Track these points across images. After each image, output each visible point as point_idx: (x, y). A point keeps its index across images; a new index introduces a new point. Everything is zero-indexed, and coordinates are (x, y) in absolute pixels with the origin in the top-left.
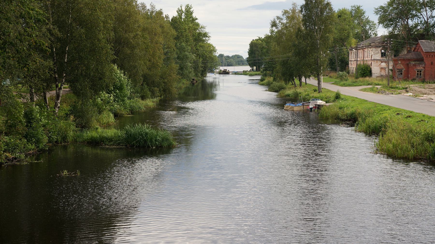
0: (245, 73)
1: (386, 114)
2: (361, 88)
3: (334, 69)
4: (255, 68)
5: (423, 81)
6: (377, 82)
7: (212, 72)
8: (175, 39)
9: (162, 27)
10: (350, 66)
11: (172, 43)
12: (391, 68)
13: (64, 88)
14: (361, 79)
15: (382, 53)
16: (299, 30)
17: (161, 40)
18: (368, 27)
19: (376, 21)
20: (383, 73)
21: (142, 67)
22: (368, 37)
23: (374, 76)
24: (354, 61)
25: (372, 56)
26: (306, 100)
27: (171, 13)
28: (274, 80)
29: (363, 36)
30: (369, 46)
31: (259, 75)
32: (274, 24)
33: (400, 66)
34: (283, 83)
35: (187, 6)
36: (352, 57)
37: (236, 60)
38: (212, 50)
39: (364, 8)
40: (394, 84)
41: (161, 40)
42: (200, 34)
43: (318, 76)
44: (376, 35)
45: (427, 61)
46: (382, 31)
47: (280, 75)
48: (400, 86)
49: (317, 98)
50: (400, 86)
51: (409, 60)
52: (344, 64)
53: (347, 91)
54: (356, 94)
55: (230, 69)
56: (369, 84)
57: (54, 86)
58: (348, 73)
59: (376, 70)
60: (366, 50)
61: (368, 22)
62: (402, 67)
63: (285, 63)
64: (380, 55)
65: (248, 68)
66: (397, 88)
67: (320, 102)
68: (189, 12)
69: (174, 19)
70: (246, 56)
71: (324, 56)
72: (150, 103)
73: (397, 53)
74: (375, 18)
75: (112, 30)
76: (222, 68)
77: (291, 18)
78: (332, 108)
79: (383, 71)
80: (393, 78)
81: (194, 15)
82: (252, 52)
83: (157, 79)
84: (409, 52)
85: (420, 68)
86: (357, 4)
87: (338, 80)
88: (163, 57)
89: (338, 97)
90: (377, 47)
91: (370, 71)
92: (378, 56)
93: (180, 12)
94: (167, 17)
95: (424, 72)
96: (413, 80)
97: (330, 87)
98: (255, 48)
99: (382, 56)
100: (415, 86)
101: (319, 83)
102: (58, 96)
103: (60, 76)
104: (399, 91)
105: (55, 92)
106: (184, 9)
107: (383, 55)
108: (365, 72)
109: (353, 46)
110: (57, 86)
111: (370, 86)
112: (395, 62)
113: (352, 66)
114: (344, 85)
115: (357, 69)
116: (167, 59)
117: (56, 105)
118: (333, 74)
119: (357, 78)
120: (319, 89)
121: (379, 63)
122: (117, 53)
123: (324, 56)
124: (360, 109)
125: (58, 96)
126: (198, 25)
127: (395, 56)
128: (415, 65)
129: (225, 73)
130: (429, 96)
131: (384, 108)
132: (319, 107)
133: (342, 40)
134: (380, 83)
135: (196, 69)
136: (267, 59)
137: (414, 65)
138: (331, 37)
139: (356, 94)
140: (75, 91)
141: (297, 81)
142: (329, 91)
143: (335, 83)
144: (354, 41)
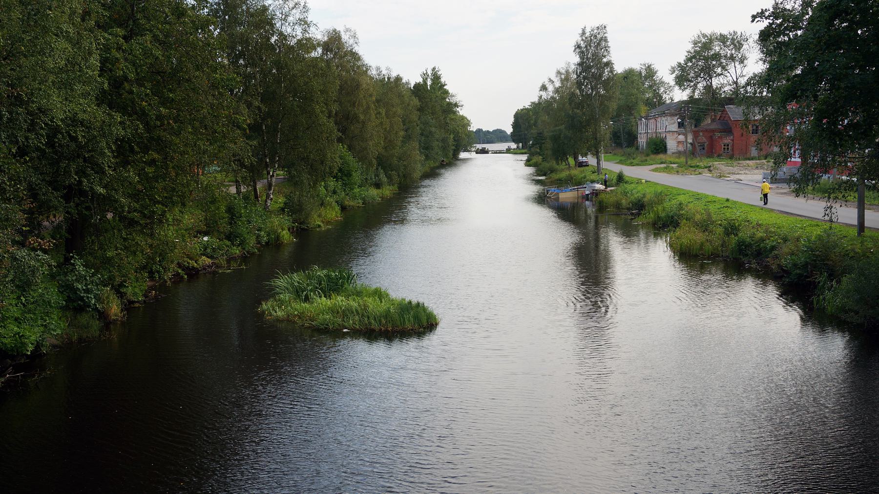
0: (508, 151)
1: (681, 198)
2: (654, 167)
3: (619, 145)
4: (521, 145)
5: (731, 158)
6: (672, 160)
7: (466, 150)
8: (419, 110)
9: (400, 96)
10: (639, 140)
11: (414, 116)
12: (690, 140)
13: (278, 175)
14: (653, 156)
15: (679, 123)
16: (573, 94)
17: (400, 111)
18: (662, 89)
19: (672, 83)
20: (681, 148)
21: (374, 146)
22: (661, 102)
23: (669, 152)
24: (644, 132)
25: (668, 126)
26: (579, 183)
27: (412, 78)
28: (544, 160)
29: (656, 104)
30: (663, 114)
31: (525, 153)
32: (544, 88)
33: (702, 139)
34: (553, 163)
35: (434, 69)
36: (641, 129)
37: (498, 136)
38: (464, 122)
39: (655, 67)
40: (695, 162)
41: (400, 111)
42: (450, 104)
43: (597, 154)
44: (672, 100)
45: (737, 132)
46: (680, 95)
47: (550, 152)
48: (701, 164)
49: (593, 182)
50: (701, 164)
51: (713, 131)
52: (631, 139)
53: (631, 172)
54: (645, 176)
55: (487, 146)
56: (662, 163)
57: (265, 172)
58: (637, 149)
59: (672, 144)
60: (659, 119)
61: (662, 83)
62: (704, 140)
63: (555, 139)
64: (676, 125)
65: (513, 146)
66: (698, 166)
67: (599, 186)
68: (436, 78)
69: (417, 86)
70: (509, 130)
71: (606, 127)
72: (388, 191)
73: (698, 122)
74: (670, 79)
75: (335, 101)
76: (480, 146)
77: (565, 79)
78: (612, 194)
79: (680, 145)
80: (693, 154)
81: (442, 80)
82: (515, 125)
83: (395, 161)
84: (713, 120)
85: (728, 140)
86: (648, 61)
87: (623, 158)
88: (402, 133)
89: (620, 178)
90: (672, 115)
91: (665, 147)
92: (674, 127)
93: (425, 76)
94: (408, 83)
95: (733, 145)
96: (719, 156)
97: (612, 166)
98: (522, 119)
99: (679, 127)
100: (720, 165)
101: (598, 163)
102: (270, 186)
103: (273, 161)
104: (700, 170)
105: (266, 181)
106: (430, 72)
107: (680, 125)
108: (658, 147)
109: (643, 114)
110: (268, 173)
111: (662, 166)
112: (696, 135)
113: (642, 140)
114: (632, 164)
115: (648, 144)
116: (408, 138)
117: (268, 196)
118: (620, 151)
119: (648, 155)
120: (598, 170)
121: (676, 135)
122: (344, 131)
123: (606, 127)
124: (649, 193)
125: (270, 186)
126: (447, 92)
127: (696, 126)
128: (720, 138)
129: (484, 151)
130: (738, 177)
131: (680, 192)
132: (596, 193)
133: (629, 109)
134: (677, 160)
135: (444, 149)
136: (534, 131)
137: (719, 137)
138: (613, 106)
139: (645, 176)
140: (292, 181)
141: (571, 161)
142: (611, 171)
143: (621, 162)
144: (643, 109)
